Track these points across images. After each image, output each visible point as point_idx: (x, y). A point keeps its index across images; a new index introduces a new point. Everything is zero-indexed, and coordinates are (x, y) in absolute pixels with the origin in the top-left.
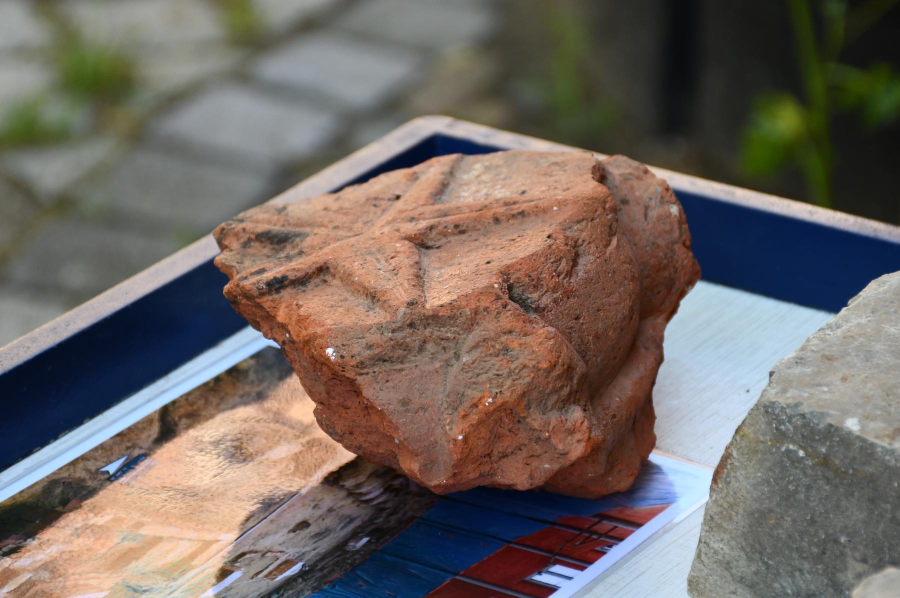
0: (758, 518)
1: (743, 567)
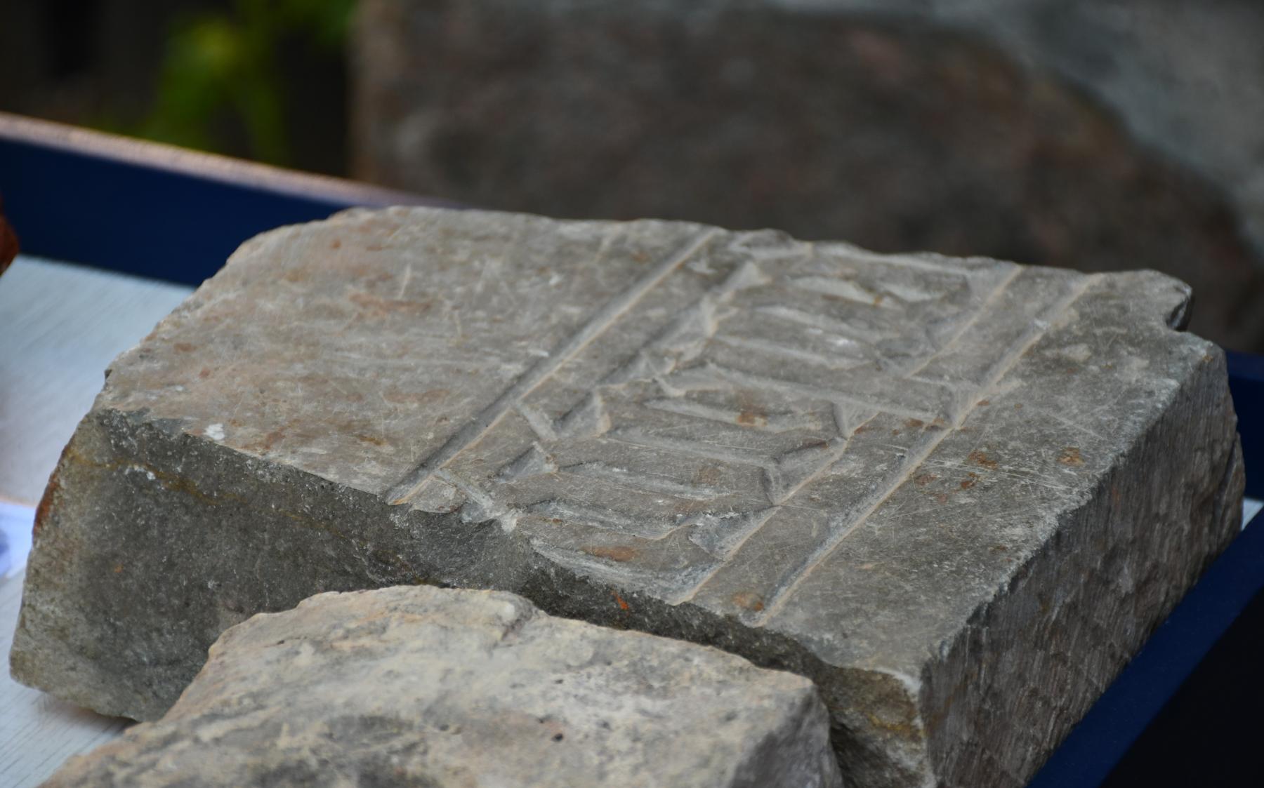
0: (99, 566)
1: (84, 633)
